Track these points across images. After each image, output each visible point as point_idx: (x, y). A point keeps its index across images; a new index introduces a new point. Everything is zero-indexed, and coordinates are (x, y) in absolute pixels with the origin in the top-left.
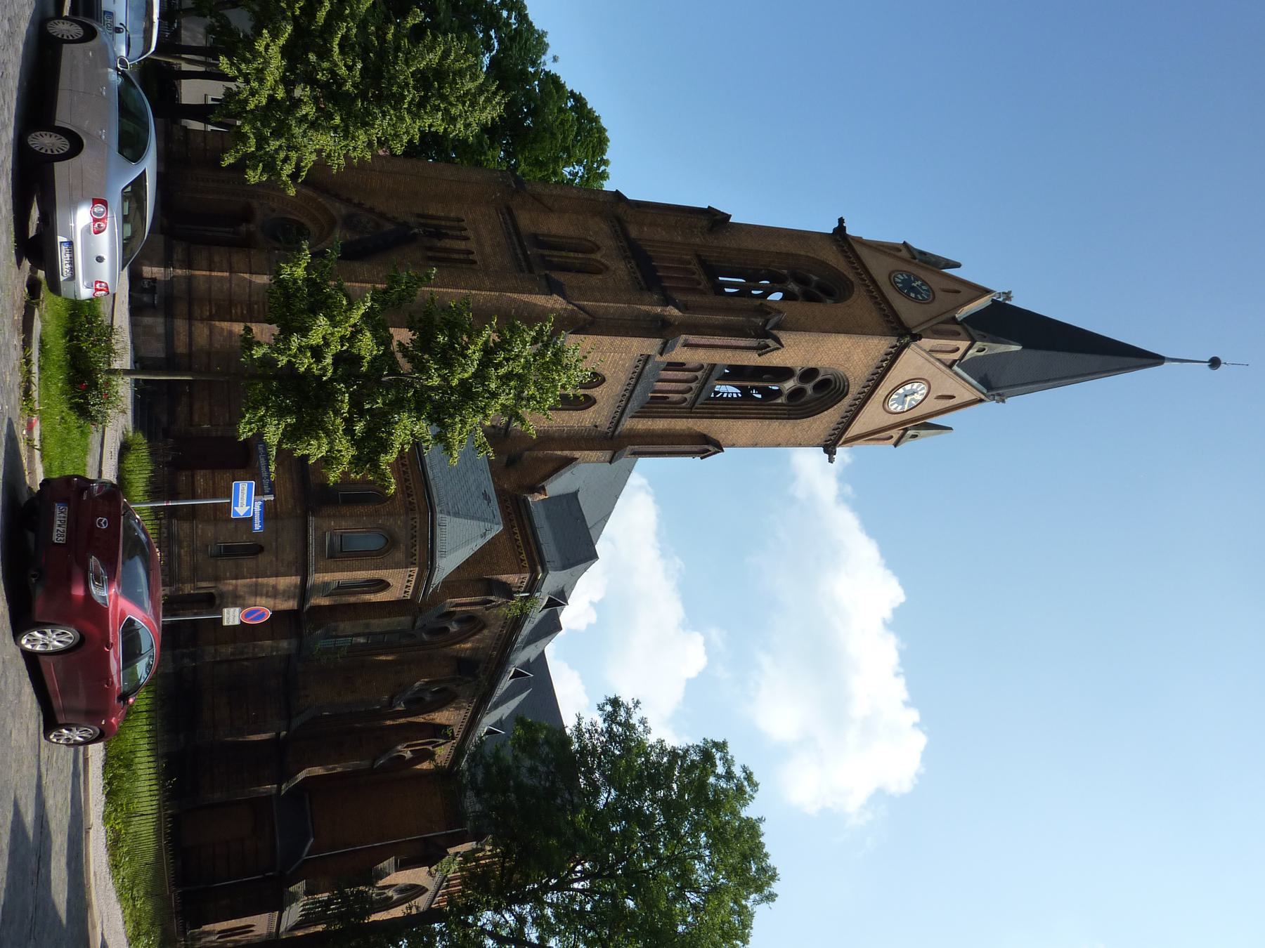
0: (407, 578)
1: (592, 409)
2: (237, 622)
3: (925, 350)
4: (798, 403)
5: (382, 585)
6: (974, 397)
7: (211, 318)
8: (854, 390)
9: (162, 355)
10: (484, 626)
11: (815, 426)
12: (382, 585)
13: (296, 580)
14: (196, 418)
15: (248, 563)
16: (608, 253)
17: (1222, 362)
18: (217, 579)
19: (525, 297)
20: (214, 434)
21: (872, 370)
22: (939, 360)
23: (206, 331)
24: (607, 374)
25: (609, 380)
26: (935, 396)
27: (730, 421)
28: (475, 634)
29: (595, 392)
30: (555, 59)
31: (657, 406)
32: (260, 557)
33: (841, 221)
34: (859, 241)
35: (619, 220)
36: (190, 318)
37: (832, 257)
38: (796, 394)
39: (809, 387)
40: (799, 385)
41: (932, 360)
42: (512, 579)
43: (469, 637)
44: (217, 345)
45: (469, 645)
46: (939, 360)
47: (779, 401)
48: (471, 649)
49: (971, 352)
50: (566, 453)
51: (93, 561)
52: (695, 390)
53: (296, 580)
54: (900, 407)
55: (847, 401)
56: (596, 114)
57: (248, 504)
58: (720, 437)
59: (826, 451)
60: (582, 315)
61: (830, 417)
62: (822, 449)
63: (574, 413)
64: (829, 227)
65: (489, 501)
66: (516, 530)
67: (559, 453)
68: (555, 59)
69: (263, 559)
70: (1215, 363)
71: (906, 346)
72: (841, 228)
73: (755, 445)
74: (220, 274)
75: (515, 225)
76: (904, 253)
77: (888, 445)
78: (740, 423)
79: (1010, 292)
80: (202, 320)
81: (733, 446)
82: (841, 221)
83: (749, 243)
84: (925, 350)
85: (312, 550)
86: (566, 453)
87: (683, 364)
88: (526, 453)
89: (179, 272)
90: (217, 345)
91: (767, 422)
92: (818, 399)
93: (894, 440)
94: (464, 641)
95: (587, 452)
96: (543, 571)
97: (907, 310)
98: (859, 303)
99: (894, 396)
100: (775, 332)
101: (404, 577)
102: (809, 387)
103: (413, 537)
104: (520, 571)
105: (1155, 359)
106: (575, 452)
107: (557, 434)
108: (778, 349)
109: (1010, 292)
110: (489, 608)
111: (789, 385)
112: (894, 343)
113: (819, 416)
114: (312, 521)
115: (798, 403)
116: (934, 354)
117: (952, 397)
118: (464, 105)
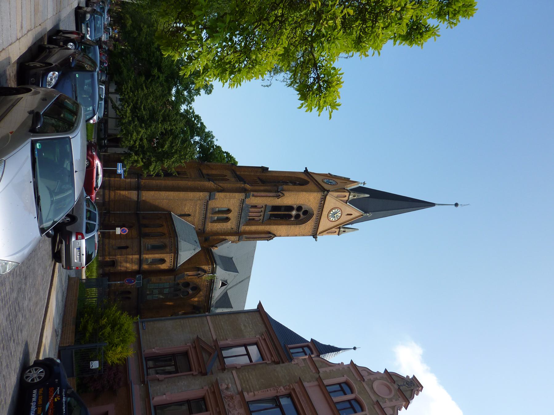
0: (170, 263)
1: (229, 222)
2: (119, 233)
3: (334, 197)
4: (299, 220)
5: (163, 261)
6: (359, 214)
7: (115, 190)
8: (315, 212)
9: (102, 201)
10: (200, 290)
11: (307, 227)
12: (163, 261)
13: (137, 256)
14: (111, 220)
15: (124, 251)
16: (228, 173)
17: (459, 204)
18: (115, 255)
19: (202, 183)
20: (115, 224)
21: (318, 205)
22: (341, 200)
23: (114, 194)
24: (232, 208)
25: (233, 211)
26: (346, 214)
27: (277, 226)
28: (197, 294)
29: (230, 215)
30: (217, 140)
31: (251, 221)
32: (128, 249)
33: (306, 168)
34: (311, 172)
35: (233, 170)
36: (109, 190)
37: (306, 178)
38: (297, 216)
39: (301, 213)
40: (297, 213)
41: (339, 200)
42: (206, 267)
43: (196, 295)
44: (116, 198)
45: (196, 299)
46: (341, 200)
47: (292, 219)
48: (198, 301)
49: (350, 197)
50: (223, 237)
51: (93, 147)
52: (262, 216)
53: (137, 256)
54: (334, 219)
55: (314, 217)
56: (411, 377)
57: (121, 170)
58: (275, 232)
59: (314, 237)
60: (220, 188)
61: (310, 224)
62: (312, 237)
63: (224, 224)
64: (303, 170)
65: (197, 243)
66: (207, 256)
67: (221, 237)
68: (217, 140)
69: (129, 250)
70: (456, 205)
71: (327, 195)
72: (306, 170)
73: (288, 236)
74: (117, 179)
75: (202, 173)
76: (329, 175)
77: (335, 236)
78: (280, 227)
79: (365, 182)
80: (112, 190)
81: (280, 236)
82: (306, 168)
83: (274, 174)
84: (334, 197)
85: (142, 248)
86: (223, 237)
87: (256, 206)
88: (211, 237)
89: (107, 178)
90: (116, 198)
91: (289, 226)
92: (305, 218)
93: (337, 233)
94: (194, 297)
95: (230, 237)
96: (215, 264)
97: (326, 187)
98: (311, 185)
99: (330, 215)
100: (282, 192)
101: (170, 258)
102: (301, 213)
103: (172, 245)
104: (208, 265)
105: (432, 205)
106: (226, 237)
107: (220, 232)
108: (283, 196)
109: (365, 182)
110: (199, 277)
111: (294, 213)
112: (323, 194)
113: (307, 223)
114: (142, 240)
115: (299, 220)
116: (338, 198)
117: (351, 215)
118: (175, 122)
